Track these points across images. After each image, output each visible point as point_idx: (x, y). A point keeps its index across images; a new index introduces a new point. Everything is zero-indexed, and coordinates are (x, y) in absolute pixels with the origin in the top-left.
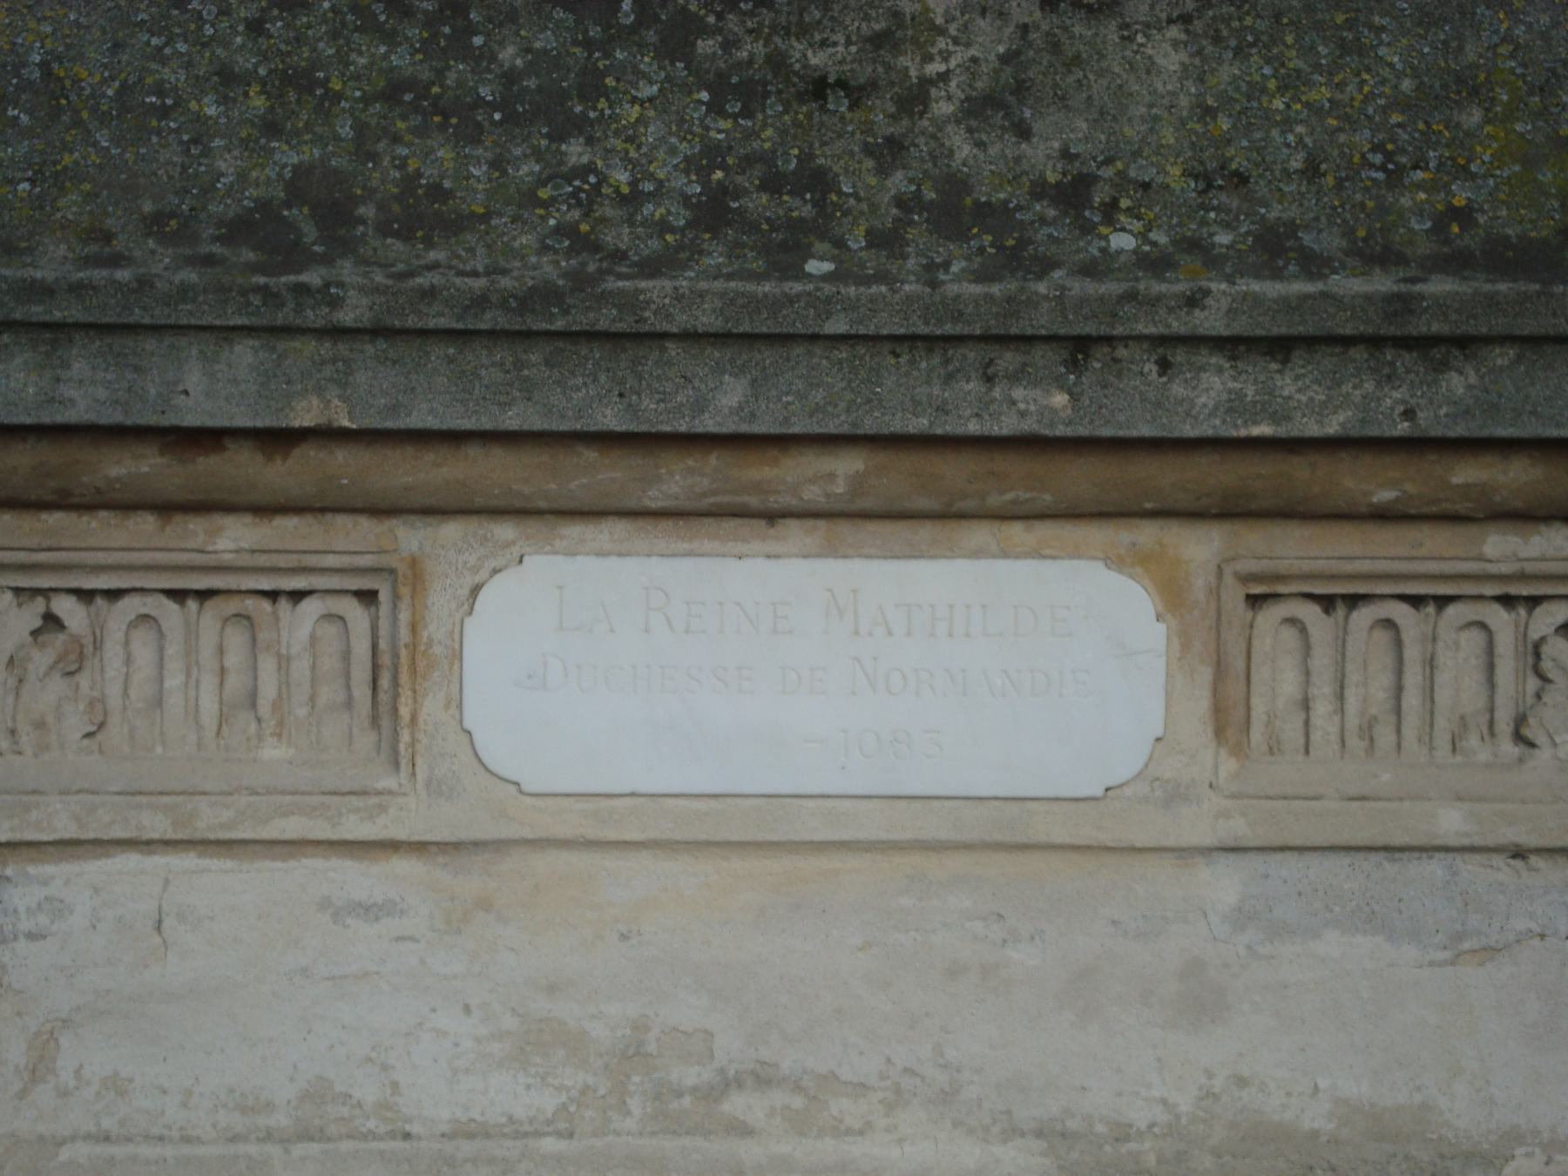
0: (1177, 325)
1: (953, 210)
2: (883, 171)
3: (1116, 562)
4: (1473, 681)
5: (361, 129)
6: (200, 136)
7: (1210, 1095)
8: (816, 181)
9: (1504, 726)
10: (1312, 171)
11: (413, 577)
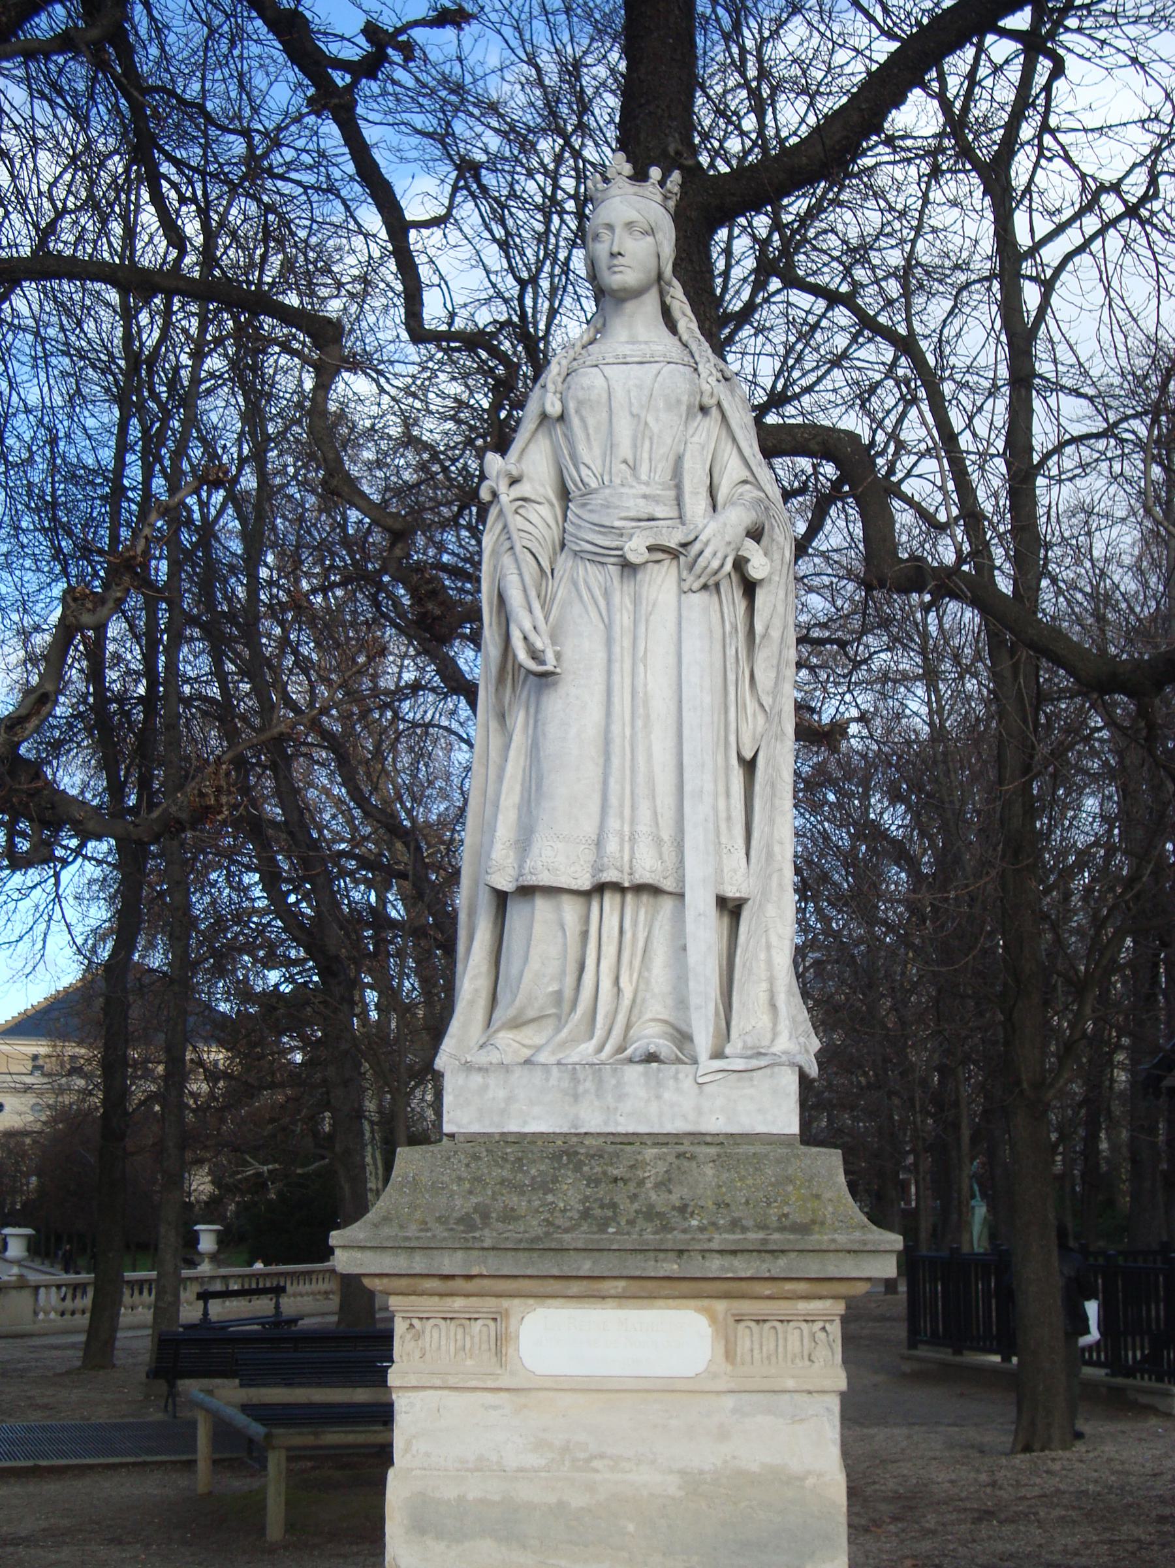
0: (706, 1246)
1: (650, 1214)
2: (632, 1202)
3: (698, 1310)
4: (798, 1343)
5: (494, 1193)
6: (452, 1194)
7: (726, 1462)
8: (614, 1206)
9: (806, 1354)
10: (747, 1203)
11: (506, 1314)
